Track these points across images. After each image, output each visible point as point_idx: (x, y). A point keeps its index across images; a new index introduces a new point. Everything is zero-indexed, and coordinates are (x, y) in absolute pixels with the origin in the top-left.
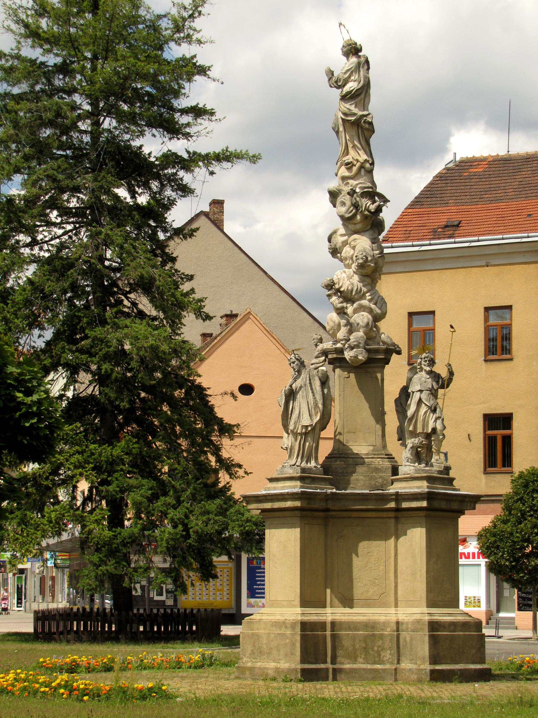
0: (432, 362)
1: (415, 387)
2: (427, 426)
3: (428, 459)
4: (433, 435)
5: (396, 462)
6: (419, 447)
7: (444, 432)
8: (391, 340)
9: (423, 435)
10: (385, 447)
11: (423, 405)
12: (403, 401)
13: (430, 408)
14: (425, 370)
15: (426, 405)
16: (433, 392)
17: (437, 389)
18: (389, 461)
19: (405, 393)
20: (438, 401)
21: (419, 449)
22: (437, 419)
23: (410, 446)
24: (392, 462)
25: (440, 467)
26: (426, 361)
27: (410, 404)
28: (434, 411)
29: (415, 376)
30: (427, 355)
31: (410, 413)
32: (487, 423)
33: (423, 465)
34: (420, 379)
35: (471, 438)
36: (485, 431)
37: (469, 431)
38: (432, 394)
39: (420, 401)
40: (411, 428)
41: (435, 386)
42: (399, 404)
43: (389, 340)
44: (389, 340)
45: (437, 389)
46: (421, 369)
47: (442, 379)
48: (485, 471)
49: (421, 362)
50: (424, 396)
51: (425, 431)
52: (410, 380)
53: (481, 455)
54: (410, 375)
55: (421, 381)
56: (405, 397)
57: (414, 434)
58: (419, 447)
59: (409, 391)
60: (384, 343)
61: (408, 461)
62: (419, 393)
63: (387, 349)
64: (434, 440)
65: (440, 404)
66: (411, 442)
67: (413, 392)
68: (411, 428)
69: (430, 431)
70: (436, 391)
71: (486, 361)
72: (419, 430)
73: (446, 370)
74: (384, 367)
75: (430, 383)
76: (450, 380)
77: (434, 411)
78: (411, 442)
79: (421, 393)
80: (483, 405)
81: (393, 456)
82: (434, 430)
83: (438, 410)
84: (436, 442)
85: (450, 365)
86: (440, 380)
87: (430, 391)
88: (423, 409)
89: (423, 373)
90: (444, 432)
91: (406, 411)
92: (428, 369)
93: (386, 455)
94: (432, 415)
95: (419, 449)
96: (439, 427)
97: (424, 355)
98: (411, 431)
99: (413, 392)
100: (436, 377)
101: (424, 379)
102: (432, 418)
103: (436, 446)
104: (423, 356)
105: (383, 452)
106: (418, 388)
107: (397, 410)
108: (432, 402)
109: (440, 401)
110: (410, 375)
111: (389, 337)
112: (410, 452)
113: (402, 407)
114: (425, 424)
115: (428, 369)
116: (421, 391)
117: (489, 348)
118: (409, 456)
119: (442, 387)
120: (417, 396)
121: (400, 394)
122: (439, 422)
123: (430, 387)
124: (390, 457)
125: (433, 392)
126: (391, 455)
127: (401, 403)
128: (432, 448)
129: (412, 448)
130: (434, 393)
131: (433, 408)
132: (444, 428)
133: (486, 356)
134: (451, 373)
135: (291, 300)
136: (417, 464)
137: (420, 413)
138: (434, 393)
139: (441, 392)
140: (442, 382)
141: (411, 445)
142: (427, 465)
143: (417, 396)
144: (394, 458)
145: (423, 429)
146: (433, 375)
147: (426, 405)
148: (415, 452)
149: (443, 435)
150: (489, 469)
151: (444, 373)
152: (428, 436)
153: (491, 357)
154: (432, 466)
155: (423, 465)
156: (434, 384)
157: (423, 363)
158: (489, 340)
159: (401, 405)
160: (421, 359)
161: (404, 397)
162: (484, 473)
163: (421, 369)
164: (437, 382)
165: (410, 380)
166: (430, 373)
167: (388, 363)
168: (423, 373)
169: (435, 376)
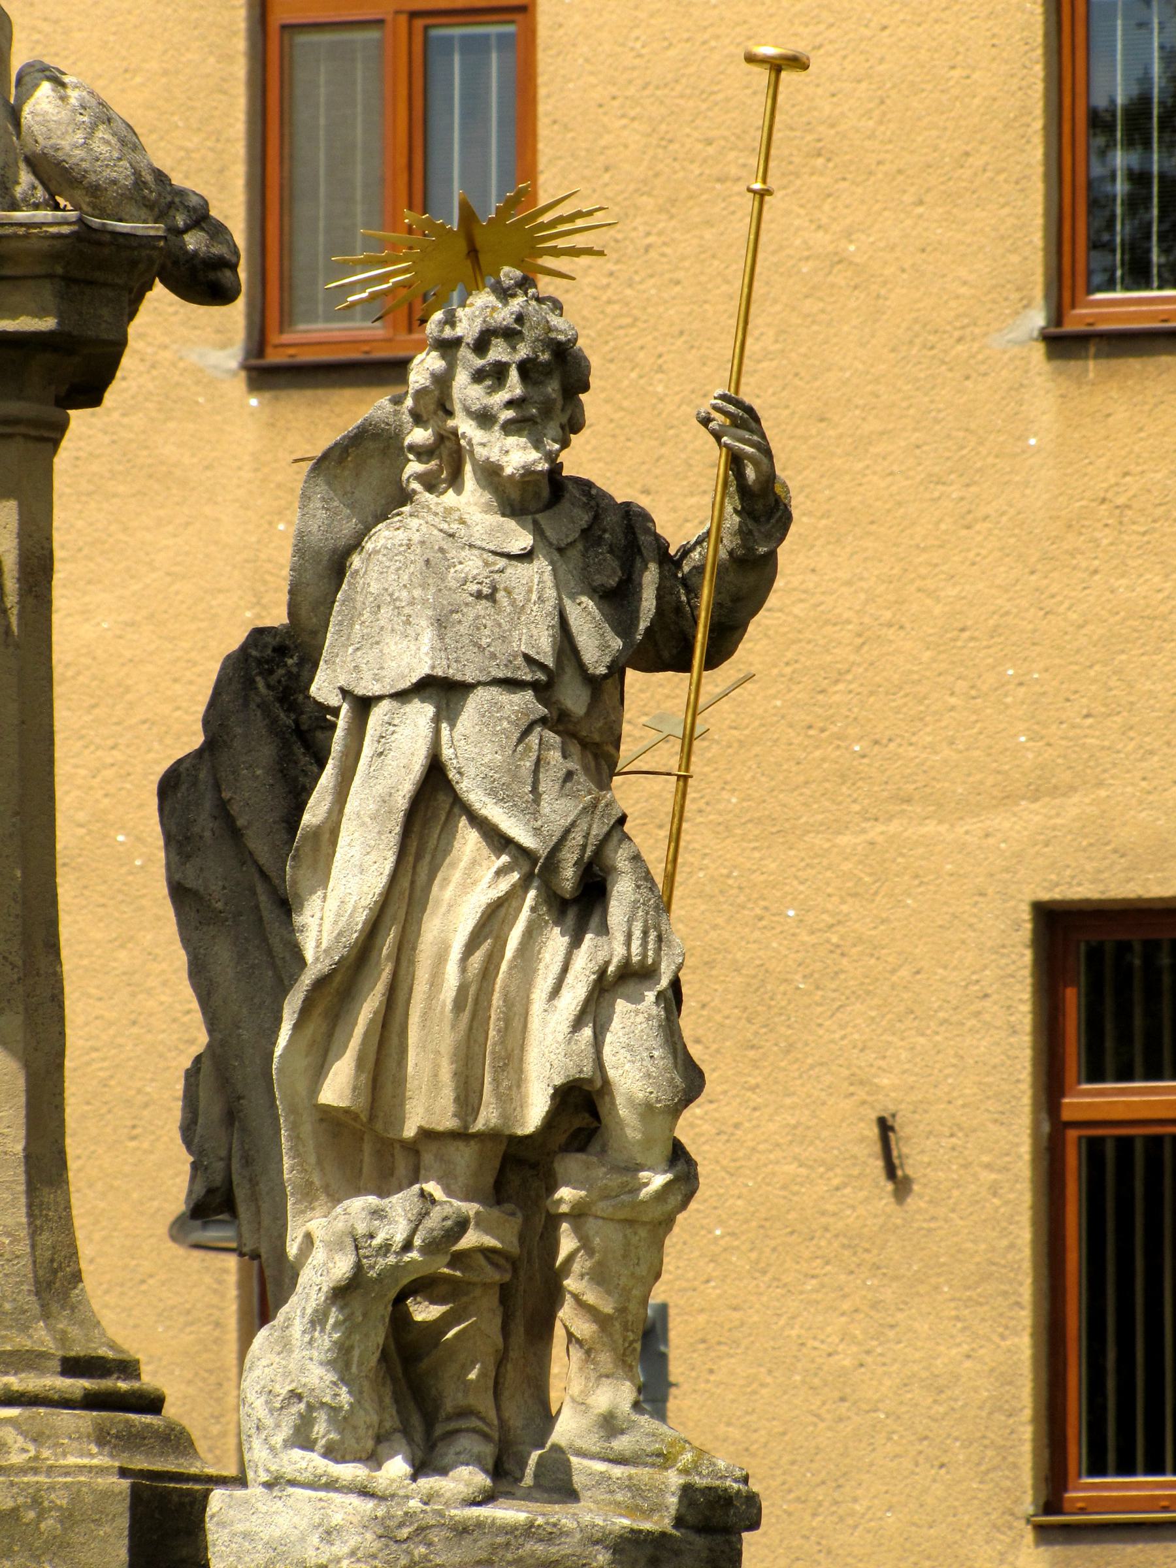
0: (555, 382)
1: (376, 649)
2: (511, 1062)
3: (516, 1413)
4: (571, 1164)
5: (177, 1440)
6: (425, 1287)
7: (692, 1128)
8: (129, 141)
9: (463, 1157)
10: (56, 1278)
11: (468, 840)
12: (252, 792)
13: (536, 868)
14: (490, 474)
15: (498, 840)
16: (574, 699)
17: (616, 671)
18: (102, 1438)
19: (271, 715)
20: (627, 793)
21: (424, 1312)
22: (607, 987)
23: (321, 1271)
24: (131, 1440)
25: (640, 1497)
26: (496, 375)
27: (331, 830)
28: (582, 901)
29: (383, 536)
30: (504, 315)
31: (327, 920)
32: (1072, 998)
33: (467, 1478)
34: (433, 566)
35: (915, 1157)
36: (1051, 1085)
37: (891, 1090)
38: (558, 721)
39: (436, 795)
40: (338, 1086)
41: (596, 643)
42: (205, 824)
43: (103, 144)
44: (103, 144)
45: (616, 671)
46: (449, 459)
47: (669, 562)
48: (1052, 1502)
49: (443, 381)
50: (478, 745)
51: (487, 1117)
52: (325, 573)
53: (1019, 1347)
54: (329, 521)
55: (440, 591)
56: (267, 752)
57: (368, 1149)
58: (425, 1287)
59: (324, 687)
60: (55, 175)
61: (302, 1439)
62: (421, 712)
63: (85, 235)
64: (578, 1214)
65: (648, 840)
66: (330, 1235)
67: (363, 705)
68: (338, 1086)
69: (534, 1111)
70: (606, 688)
71: (1062, 343)
72: (427, 1105)
73: (705, 459)
74: (52, 434)
75: (537, 604)
76: (749, 574)
77: (582, 901)
78: (330, 1235)
79: (447, 713)
80: (1032, 815)
81: (150, 1379)
82: (581, 1105)
83: (623, 893)
84: (604, 1235)
85: (745, 418)
86: (650, 578)
87: (542, 690)
88: (470, 882)
89: (470, 501)
90: (692, 1128)
91: (287, 907)
92: (517, 455)
93: (73, 1367)
94: (556, 941)
95: (424, 1312)
96: (631, 1069)
97: (477, 311)
98: (327, 1115)
99: (363, 705)
100: (597, 537)
101: (472, 564)
102: (563, 967)
103: (598, 1276)
104: (467, 326)
105: (41, 1337)
106: (413, 655)
107: (179, 892)
108: (558, 810)
109: (638, 797)
110: (329, 521)
111: (104, 116)
112: (326, 1340)
113: (245, 857)
114: (486, 1034)
115: (517, 455)
116: (442, 691)
117: (1098, 203)
118: (317, 1377)
119: (666, 649)
120: (399, 746)
121: (216, 719)
122: (632, 1018)
123: (544, 646)
124: (112, 1392)
125: (574, 699)
126: (128, 1368)
127: (223, 812)
128: (553, 1294)
129: (342, 1294)
130: (575, 716)
131: (568, 874)
132: (690, 1081)
133: (1061, 291)
134: (762, 508)
135: (750, 326)
136: (397, 1467)
137: (432, 929)
138: (575, 716)
139: (650, 696)
140: (665, 599)
141: (342, 1267)
142: (503, 1475)
143: (399, 746)
144: (152, 1403)
145: (468, 1099)
146: (568, 522)
147: (498, 840)
148: (378, 1336)
149: (678, 1156)
150: (1093, 1491)
151: (686, 509)
152: (516, 1171)
153: (1119, 305)
154: (558, 1485)
155: (467, 1478)
156: (585, 618)
157: (466, 390)
158: (1100, 122)
159: (235, 833)
160: (448, 347)
161: (256, 758)
162: (1045, 1533)
163: (449, 459)
164: (617, 600)
165: (325, 573)
166: (542, 497)
167: (90, 391)
168: (470, 501)
169: (590, 536)
